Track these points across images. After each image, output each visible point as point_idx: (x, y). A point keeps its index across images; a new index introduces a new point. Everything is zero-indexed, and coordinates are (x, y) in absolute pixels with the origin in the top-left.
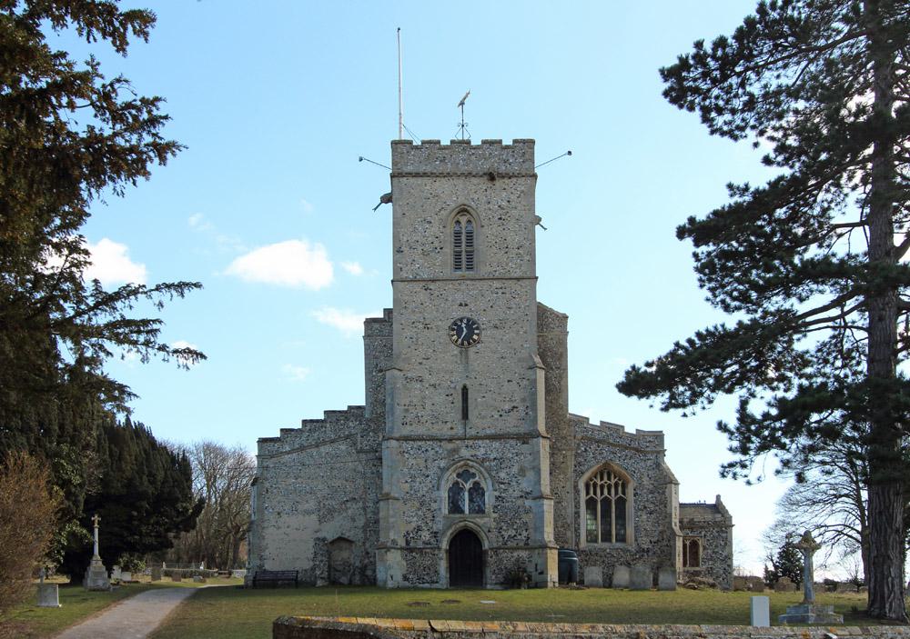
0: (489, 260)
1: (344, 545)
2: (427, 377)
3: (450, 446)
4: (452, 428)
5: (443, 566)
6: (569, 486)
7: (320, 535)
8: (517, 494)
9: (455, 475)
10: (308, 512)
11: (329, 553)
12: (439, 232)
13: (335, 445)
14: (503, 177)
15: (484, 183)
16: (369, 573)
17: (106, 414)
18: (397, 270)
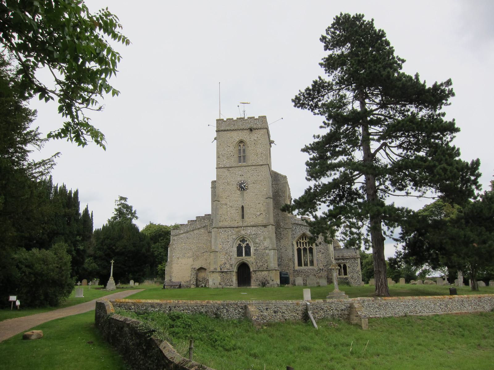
0: (252, 158)
1: (203, 271)
2: (229, 203)
3: (237, 230)
4: (238, 223)
5: (234, 279)
6: (290, 244)
7: (194, 267)
8: (263, 248)
9: (239, 241)
10: (188, 257)
11: (197, 274)
12: (232, 149)
14: (255, 129)
16: (372, 277)
17: (128, 219)
18: (218, 164)
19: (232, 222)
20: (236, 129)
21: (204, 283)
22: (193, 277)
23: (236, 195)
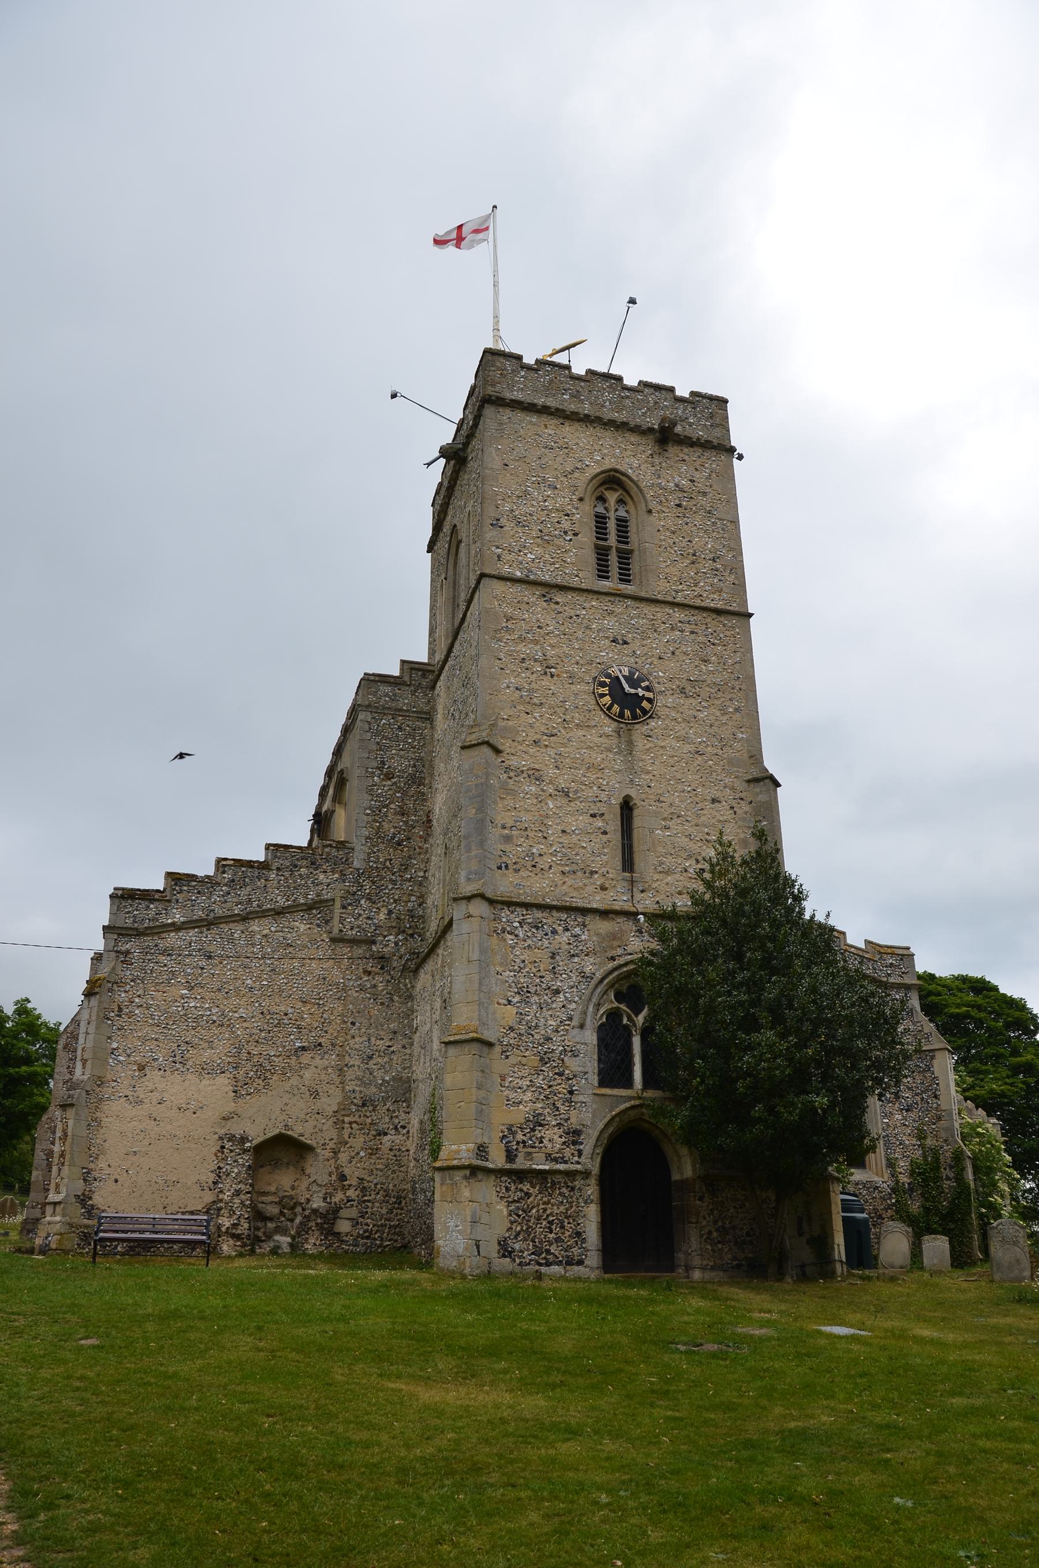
3: (604, 926)
10: (205, 1070)
13: (284, 921)
15: (648, 446)
19: (570, 881)
20: (587, 416)
21: (284, 1232)
22: (238, 1193)
23: (592, 737)
